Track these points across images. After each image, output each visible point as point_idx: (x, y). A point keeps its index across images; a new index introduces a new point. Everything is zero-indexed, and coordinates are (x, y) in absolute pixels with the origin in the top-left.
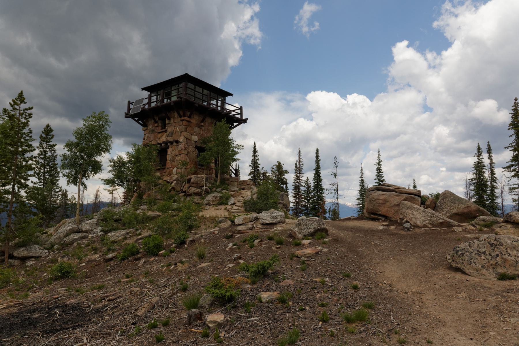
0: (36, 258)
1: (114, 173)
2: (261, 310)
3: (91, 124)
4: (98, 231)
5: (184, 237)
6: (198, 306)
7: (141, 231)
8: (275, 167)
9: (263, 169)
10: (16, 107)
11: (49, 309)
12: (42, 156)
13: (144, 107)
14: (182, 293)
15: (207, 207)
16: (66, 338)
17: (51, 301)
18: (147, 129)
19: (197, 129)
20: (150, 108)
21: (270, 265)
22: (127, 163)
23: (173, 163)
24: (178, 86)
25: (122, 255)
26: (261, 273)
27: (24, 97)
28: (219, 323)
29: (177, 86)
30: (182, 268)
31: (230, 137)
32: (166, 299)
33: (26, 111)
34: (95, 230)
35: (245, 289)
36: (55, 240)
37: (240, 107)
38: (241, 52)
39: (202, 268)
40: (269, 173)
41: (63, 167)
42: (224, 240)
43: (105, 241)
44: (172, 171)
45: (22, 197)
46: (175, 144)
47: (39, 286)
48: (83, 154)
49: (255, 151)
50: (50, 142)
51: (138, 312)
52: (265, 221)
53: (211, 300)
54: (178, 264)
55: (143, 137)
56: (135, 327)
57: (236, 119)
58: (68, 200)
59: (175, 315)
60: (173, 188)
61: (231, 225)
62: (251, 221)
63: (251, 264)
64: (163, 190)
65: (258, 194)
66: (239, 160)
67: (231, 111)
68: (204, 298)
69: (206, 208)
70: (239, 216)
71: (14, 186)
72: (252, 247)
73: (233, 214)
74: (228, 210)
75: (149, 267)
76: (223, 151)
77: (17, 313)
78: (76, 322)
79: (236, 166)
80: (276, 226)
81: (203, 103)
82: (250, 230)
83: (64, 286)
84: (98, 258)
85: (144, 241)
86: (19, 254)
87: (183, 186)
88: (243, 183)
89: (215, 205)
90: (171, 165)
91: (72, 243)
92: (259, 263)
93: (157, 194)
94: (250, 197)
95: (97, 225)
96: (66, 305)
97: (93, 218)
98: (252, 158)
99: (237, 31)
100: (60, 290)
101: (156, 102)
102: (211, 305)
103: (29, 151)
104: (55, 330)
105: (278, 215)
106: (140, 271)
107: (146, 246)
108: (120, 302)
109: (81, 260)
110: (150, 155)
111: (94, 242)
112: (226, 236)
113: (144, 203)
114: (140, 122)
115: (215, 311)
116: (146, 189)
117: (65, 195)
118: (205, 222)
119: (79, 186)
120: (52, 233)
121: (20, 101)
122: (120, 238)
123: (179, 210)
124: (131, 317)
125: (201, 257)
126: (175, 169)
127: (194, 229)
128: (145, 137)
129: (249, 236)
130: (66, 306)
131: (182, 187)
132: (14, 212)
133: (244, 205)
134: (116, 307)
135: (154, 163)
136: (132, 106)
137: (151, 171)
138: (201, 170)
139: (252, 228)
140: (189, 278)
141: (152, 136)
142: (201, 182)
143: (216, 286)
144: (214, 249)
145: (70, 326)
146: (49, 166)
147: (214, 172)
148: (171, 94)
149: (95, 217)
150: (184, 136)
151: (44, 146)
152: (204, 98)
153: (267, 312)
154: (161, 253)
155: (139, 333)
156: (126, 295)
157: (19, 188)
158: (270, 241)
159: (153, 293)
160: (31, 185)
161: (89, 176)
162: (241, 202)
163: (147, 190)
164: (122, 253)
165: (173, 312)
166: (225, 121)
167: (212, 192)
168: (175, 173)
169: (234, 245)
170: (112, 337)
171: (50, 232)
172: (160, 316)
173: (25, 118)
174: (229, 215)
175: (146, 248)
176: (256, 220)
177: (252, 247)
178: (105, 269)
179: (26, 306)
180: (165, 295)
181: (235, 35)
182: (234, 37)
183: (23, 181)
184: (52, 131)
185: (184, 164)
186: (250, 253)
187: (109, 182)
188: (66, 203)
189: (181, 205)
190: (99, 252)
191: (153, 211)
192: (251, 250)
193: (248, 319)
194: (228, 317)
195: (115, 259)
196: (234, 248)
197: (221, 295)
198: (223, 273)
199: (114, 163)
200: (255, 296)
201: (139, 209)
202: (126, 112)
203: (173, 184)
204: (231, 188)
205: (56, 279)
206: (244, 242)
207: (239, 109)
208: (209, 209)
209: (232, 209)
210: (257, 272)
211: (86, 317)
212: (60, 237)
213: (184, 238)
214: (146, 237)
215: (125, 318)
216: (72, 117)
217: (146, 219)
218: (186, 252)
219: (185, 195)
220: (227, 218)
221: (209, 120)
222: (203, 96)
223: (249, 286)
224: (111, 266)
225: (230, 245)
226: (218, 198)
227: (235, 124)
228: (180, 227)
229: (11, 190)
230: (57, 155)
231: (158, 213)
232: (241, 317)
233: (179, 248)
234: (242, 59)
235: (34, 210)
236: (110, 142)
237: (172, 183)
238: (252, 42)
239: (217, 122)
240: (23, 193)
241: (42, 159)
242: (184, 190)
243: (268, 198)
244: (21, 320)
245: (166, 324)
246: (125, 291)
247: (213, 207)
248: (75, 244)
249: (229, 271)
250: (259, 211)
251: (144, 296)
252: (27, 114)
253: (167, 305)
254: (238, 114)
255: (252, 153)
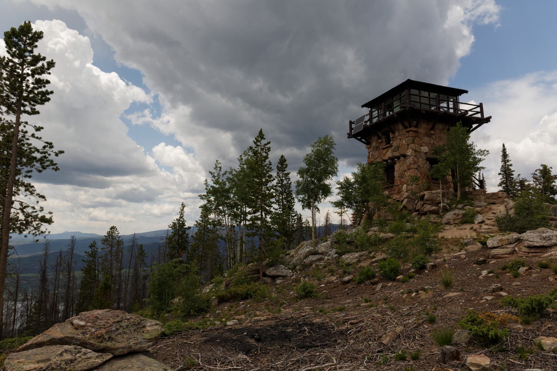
0: (284, 277)
1: (342, 195)
2: (545, 360)
3: (318, 150)
4: (333, 252)
5: (423, 261)
6: (452, 342)
7: (375, 254)
8: (538, 173)
9: (520, 176)
10: (259, 144)
11: (299, 325)
12: (280, 185)
13: (366, 125)
14: (430, 325)
15: (447, 227)
16: (317, 355)
17: (300, 318)
18: (371, 147)
19: (426, 139)
20: (372, 124)
21: (551, 301)
22: (354, 184)
23: (402, 179)
24: (400, 96)
25: (358, 279)
26: (536, 311)
27: (263, 133)
28: (484, 367)
29: (399, 95)
30: (426, 297)
31: (469, 142)
32: (412, 329)
33: (266, 146)
34: (330, 252)
35: (514, 329)
36: (296, 261)
37: (479, 105)
38: (473, 37)
39: (450, 298)
40: (530, 181)
41: (298, 193)
42: (474, 265)
43: (340, 263)
44: (402, 188)
45: (268, 222)
46: (402, 158)
47: (288, 303)
48: (313, 179)
49: (505, 155)
50: (285, 171)
51: (383, 340)
52: (532, 243)
53: (467, 337)
54: (420, 292)
55: (367, 156)
56: (382, 356)
57: (474, 120)
58: (302, 223)
59: (424, 349)
60: (404, 207)
61: (482, 248)
62: (510, 243)
63: (520, 298)
64: (394, 209)
65: (516, 208)
66: (483, 168)
67: (467, 112)
68: (459, 334)
69: (446, 228)
70: (492, 237)
71: (262, 213)
72: (516, 276)
73: (483, 234)
74: (475, 230)
75: (388, 293)
76: (461, 160)
77: (275, 326)
78: (323, 341)
79: (479, 176)
80: (549, 250)
81: (430, 108)
82: (510, 254)
83: (308, 305)
84: (336, 280)
85: (379, 265)
86: (270, 273)
87: (416, 204)
88: (492, 196)
89: (457, 224)
90: (400, 182)
91: (311, 264)
92: (533, 298)
93: (388, 214)
94: (505, 213)
95: (332, 247)
96: (313, 323)
97: (327, 241)
98: (501, 164)
99: (465, 13)
100: (306, 309)
101: (378, 116)
102: (469, 343)
103: (270, 181)
104: (307, 346)
105: (553, 236)
106: (378, 296)
107: (382, 270)
108: (362, 327)
109: (320, 281)
110: (376, 173)
111: (330, 264)
112: (477, 261)
113: (374, 224)
114: (363, 140)
115: (476, 352)
116: (375, 210)
117: (300, 219)
118: (447, 245)
119: (313, 210)
120: (293, 255)
121: (260, 138)
122: (354, 261)
123: (414, 231)
124: (376, 344)
125: (448, 285)
126: (405, 186)
127: (434, 252)
128: (369, 155)
129: (509, 262)
130: (313, 324)
131: (415, 205)
132: (263, 235)
133: (498, 223)
134: (359, 331)
135: (381, 181)
136: (353, 126)
137: (379, 190)
138: (435, 185)
139: (513, 252)
140: (436, 309)
141: (376, 153)
142: (437, 198)
143: (473, 321)
144: (463, 276)
145: (319, 344)
146: (286, 193)
147: (452, 185)
148: (393, 105)
149: (328, 239)
150: (412, 149)
151: (281, 175)
152: (431, 102)
153: (554, 364)
154: (399, 279)
155: (386, 362)
156: (367, 321)
157: (266, 214)
158: (543, 269)
159: (396, 321)
160: (274, 211)
161: (320, 200)
162: (493, 220)
163: (376, 211)
164: (357, 276)
165: (422, 345)
166: (461, 125)
167: (451, 209)
168: (405, 191)
169: (489, 273)
170: (360, 362)
171: (292, 254)
172: (407, 347)
173: (266, 153)
174: (477, 236)
175: (382, 272)
176: (517, 242)
177: (516, 276)
178: (343, 291)
179: (281, 320)
180: (409, 325)
181: (462, 19)
182: (461, 22)
183: (267, 208)
184: (285, 161)
185: (415, 179)
186: (515, 284)
187: (338, 204)
188: (301, 226)
189: (415, 225)
190: (335, 274)
191: (385, 232)
192: (516, 280)
193: (525, 369)
194: (496, 362)
195: (352, 282)
196: (490, 277)
197: (482, 333)
198: (479, 306)
199: (341, 186)
200: (532, 340)
201: (369, 231)
202: (349, 132)
203: (404, 202)
204: (477, 203)
205: (301, 298)
206: (504, 269)
207: (478, 106)
208: (450, 229)
209: (480, 229)
210: (531, 309)
211: (332, 338)
212: (300, 259)
213: (424, 263)
214: (381, 260)
215: (369, 345)
216: (300, 145)
217: (379, 241)
218: (428, 279)
219: (419, 214)
220: (475, 239)
221: (440, 126)
222: (420, 99)
223: (519, 326)
224: (348, 289)
225: (484, 273)
226: (461, 216)
227: (474, 126)
228: (417, 250)
229: (260, 216)
230: (291, 183)
231: (390, 235)
232: (513, 364)
233: (419, 274)
234: (474, 46)
235: (277, 234)
236: (336, 165)
237: (402, 201)
238: (486, 21)
239: (450, 127)
240: (268, 219)
241: (280, 187)
242: (417, 209)
243: (532, 213)
244: (279, 332)
245: (415, 358)
246: (366, 316)
247: (455, 226)
248: (314, 266)
249: (487, 305)
250: (522, 230)
251: (386, 324)
252: (266, 149)
253: (413, 336)
254: (478, 113)
255: (500, 159)
